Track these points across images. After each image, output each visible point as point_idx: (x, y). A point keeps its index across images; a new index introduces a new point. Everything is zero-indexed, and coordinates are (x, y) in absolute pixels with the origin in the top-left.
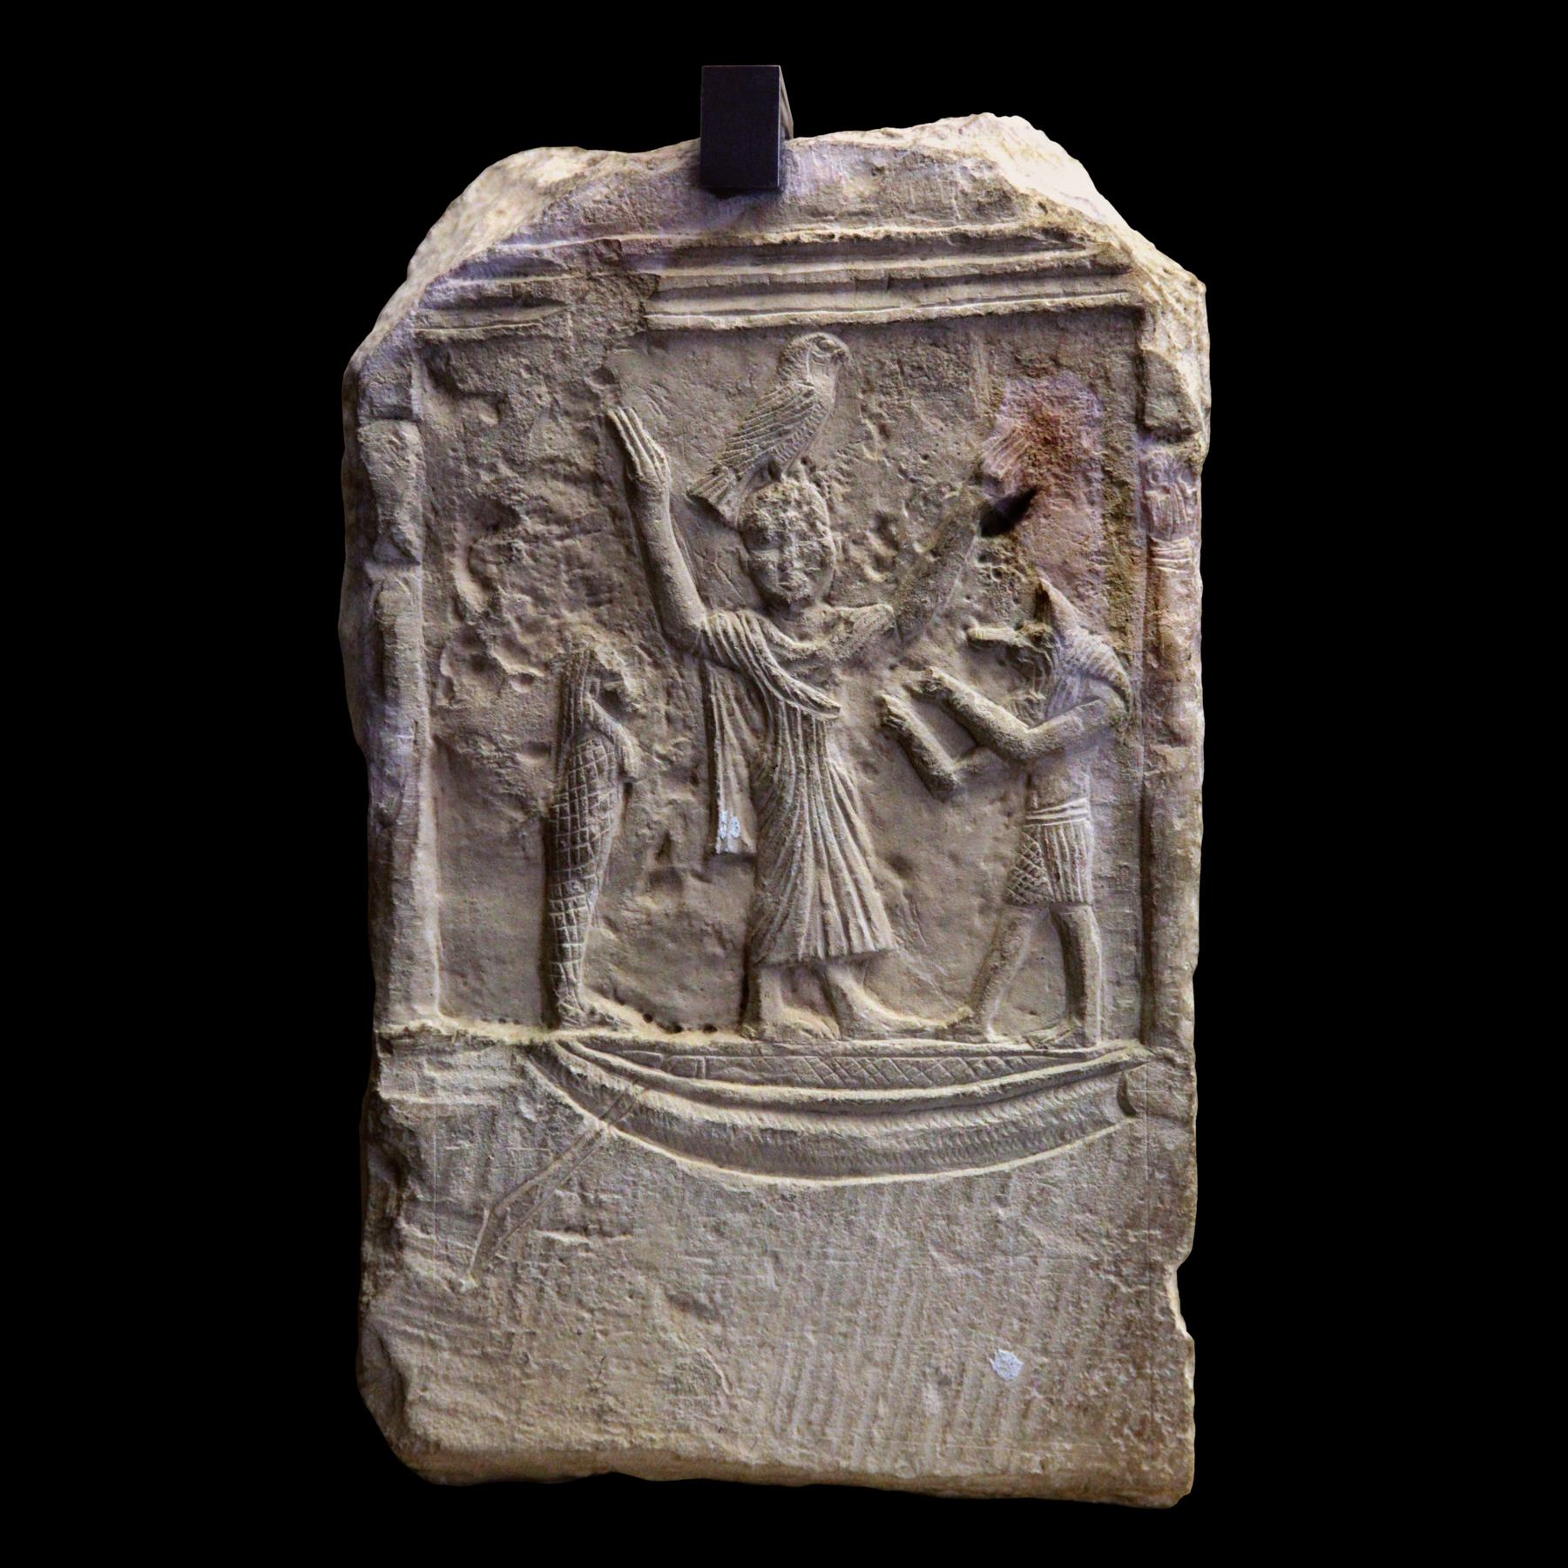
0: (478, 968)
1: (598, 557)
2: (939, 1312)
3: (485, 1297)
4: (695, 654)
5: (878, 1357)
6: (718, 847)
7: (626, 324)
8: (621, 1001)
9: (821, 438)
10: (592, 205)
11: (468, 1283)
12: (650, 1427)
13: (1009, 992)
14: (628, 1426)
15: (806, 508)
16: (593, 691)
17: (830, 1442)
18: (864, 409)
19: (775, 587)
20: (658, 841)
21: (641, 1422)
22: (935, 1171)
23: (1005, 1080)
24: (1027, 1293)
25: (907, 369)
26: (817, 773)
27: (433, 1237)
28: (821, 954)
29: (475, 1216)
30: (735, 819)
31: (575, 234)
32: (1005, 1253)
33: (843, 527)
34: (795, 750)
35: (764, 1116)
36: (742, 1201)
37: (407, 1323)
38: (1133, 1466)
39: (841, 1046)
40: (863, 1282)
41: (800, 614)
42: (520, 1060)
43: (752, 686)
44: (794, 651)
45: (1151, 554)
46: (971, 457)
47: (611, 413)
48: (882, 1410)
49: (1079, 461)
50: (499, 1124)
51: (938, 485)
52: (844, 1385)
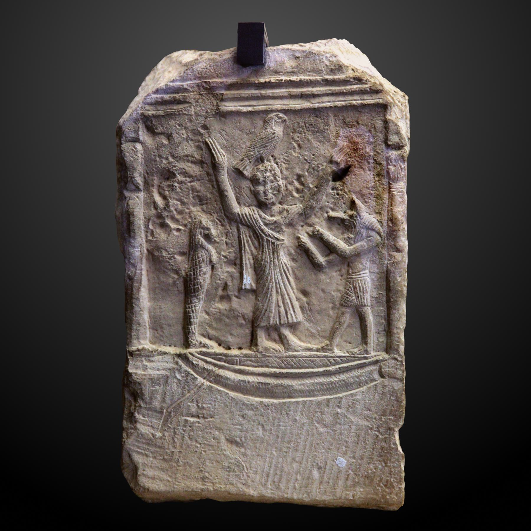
0: (162, 328)
1: (202, 189)
2: (318, 444)
3: (164, 439)
4: (236, 221)
5: (297, 459)
6: (243, 287)
7: (212, 110)
8: (210, 339)
9: (278, 148)
10: (201, 69)
11: (159, 434)
12: (220, 483)
13: (342, 336)
14: (213, 483)
15: (273, 172)
16: (201, 234)
17: (281, 488)
18: (293, 138)
19: (263, 199)
20: (223, 285)
21: (217, 481)
22: (317, 397)
23: (341, 366)
24: (348, 438)
25: (307, 125)
26: (277, 262)
27: (147, 419)
28: (278, 323)
29: (161, 412)
30: (249, 278)
31: (195, 79)
32: (340, 424)
33: (286, 178)
34: (269, 254)
35: (259, 378)
36: (251, 407)
37: (138, 448)
38: (384, 497)
39: (285, 354)
40: (292, 434)
41: (271, 208)
42: (176, 359)
43: (255, 232)
44: (269, 220)
45: (390, 188)
46: (329, 155)
47: (207, 140)
48: (299, 477)
49: (365, 156)
50: (169, 381)
51: (318, 164)
52: (286, 469)
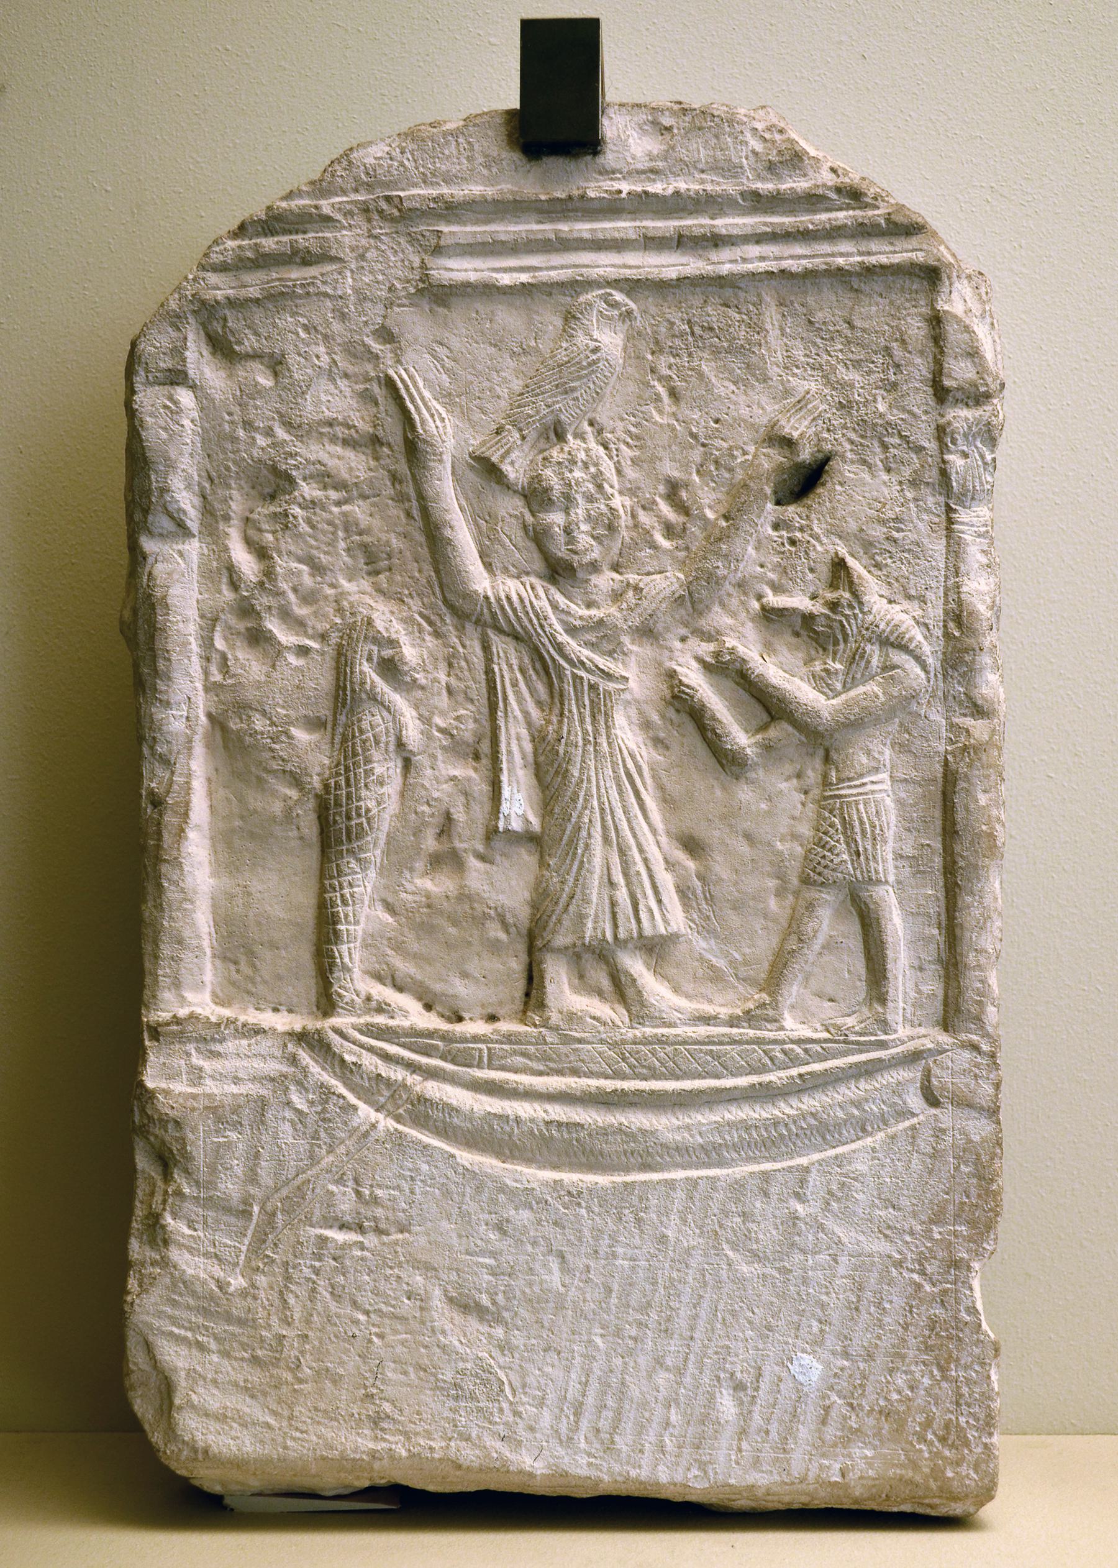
0: (251, 954)
1: (376, 523)
2: (734, 1314)
3: (255, 1298)
4: (477, 622)
5: (669, 1361)
6: (501, 825)
7: (408, 282)
8: (400, 989)
9: (608, 399)
10: (373, 161)
11: (237, 1282)
12: (429, 1435)
13: (807, 979)
14: (406, 1434)
15: (593, 470)
16: (369, 659)
17: (620, 1451)
18: (652, 371)
19: (560, 549)
20: (438, 820)
21: (419, 1429)
22: (731, 1166)
23: (803, 1070)
24: (827, 1294)
25: (697, 330)
26: (605, 745)
27: (201, 1234)
28: (609, 936)
29: (244, 1212)
30: (518, 796)
31: (356, 191)
32: (804, 1252)
33: (631, 491)
34: (582, 721)
35: (548, 1107)
36: (526, 1198)
37: (174, 1324)
38: (936, 1473)
39: (630, 1034)
40: (655, 1283)
41: (587, 581)
42: (291, 1047)
43: (537, 654)
44: (581, 618)
45: (950, 521)
46: (765, 420)
47: (391, 372)
48: (674, 1417)
49: (875, 425)
50: (269, 1115)
51: (730, 449)
52: (635, 1392)
